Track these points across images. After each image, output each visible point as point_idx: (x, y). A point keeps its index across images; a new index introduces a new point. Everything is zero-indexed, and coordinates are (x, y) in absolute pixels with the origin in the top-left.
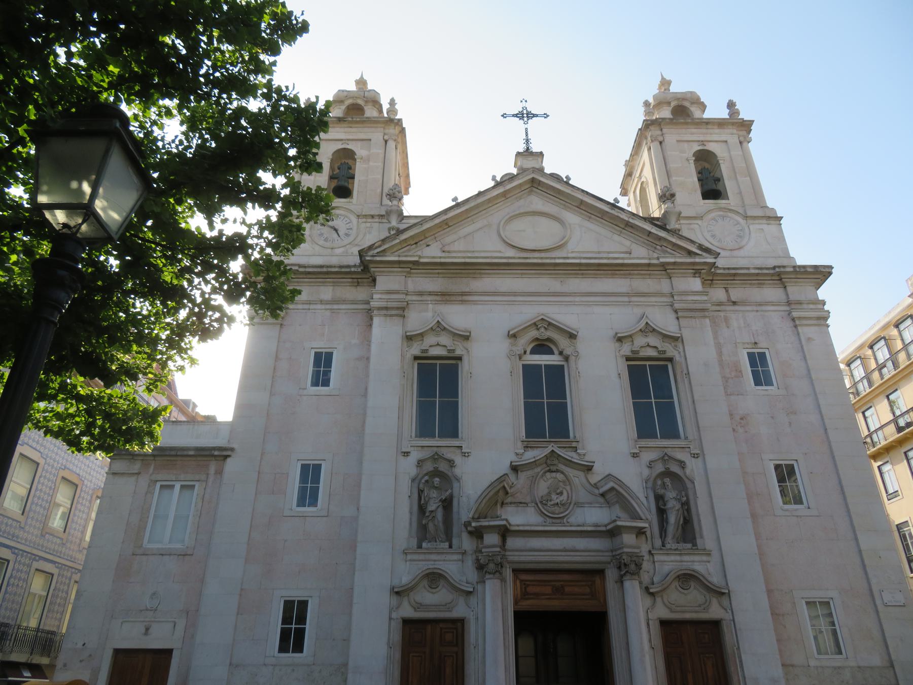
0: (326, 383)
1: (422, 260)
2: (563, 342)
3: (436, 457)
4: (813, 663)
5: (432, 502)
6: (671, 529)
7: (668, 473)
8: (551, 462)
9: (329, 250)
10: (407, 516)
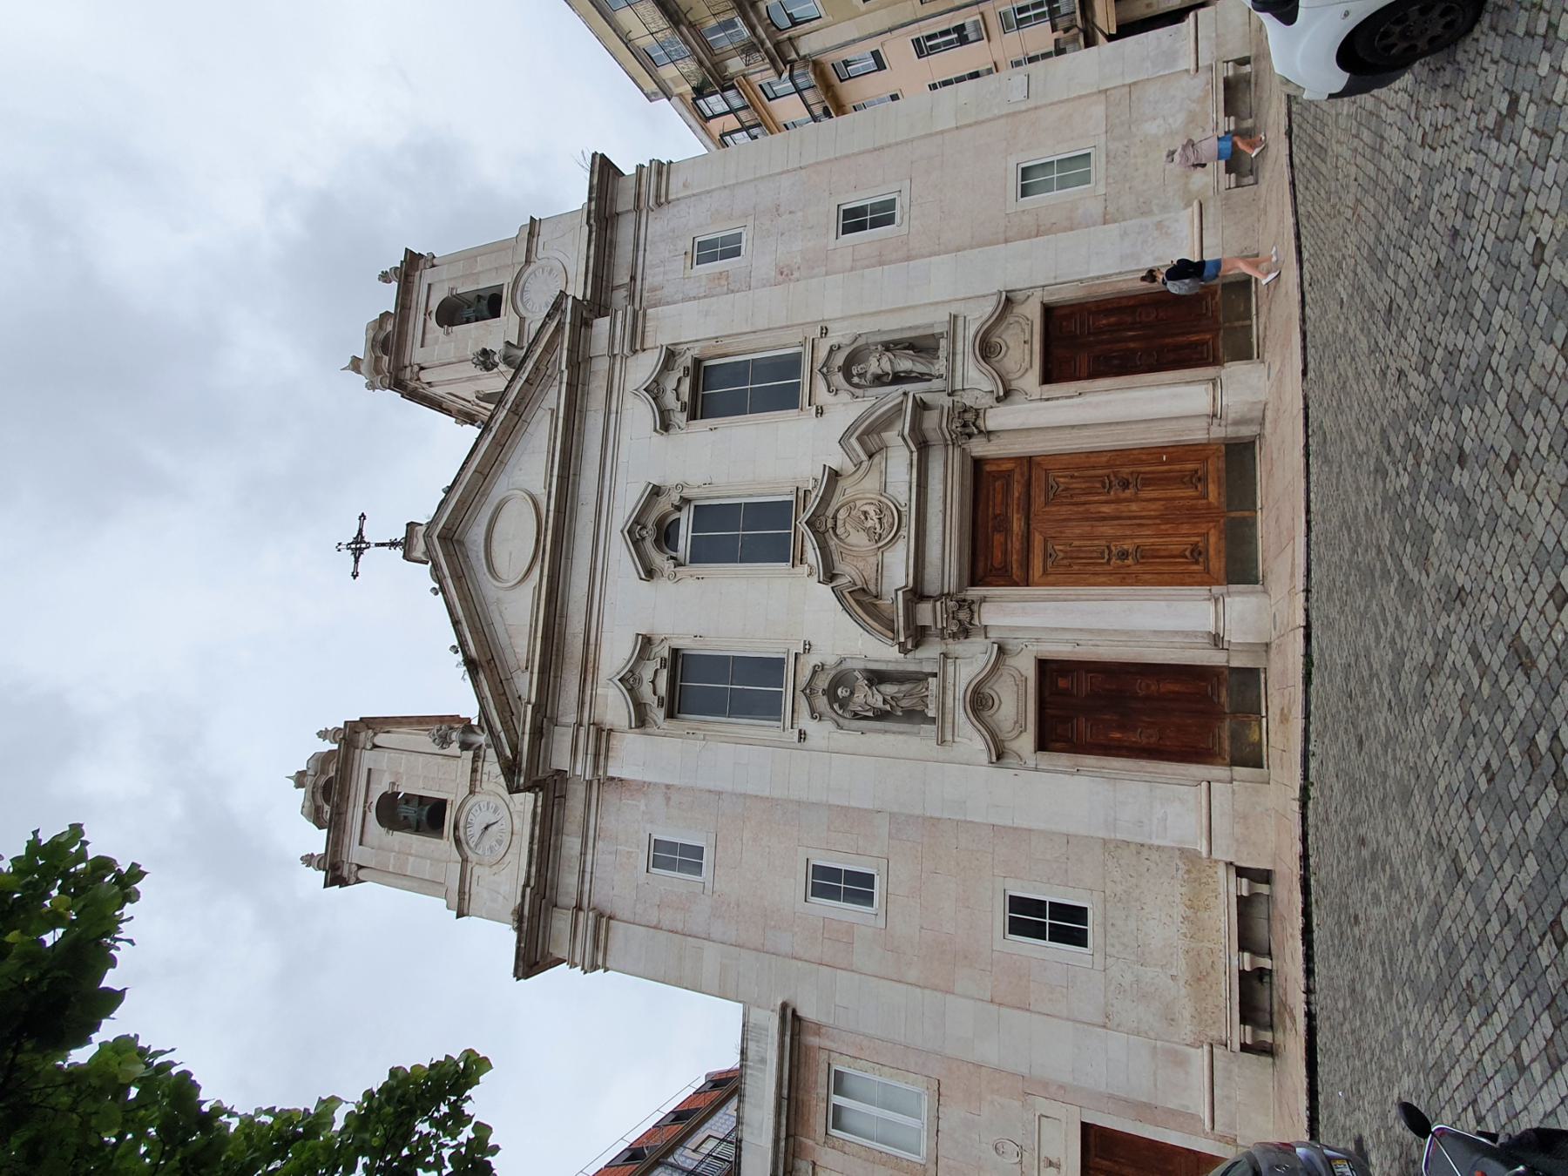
0: (698, 852)
2: (664, 505)
3: (809, 691)
4: (1102, 190)
6: (920, 368)
7: (846, 370)
10: (890, 737)
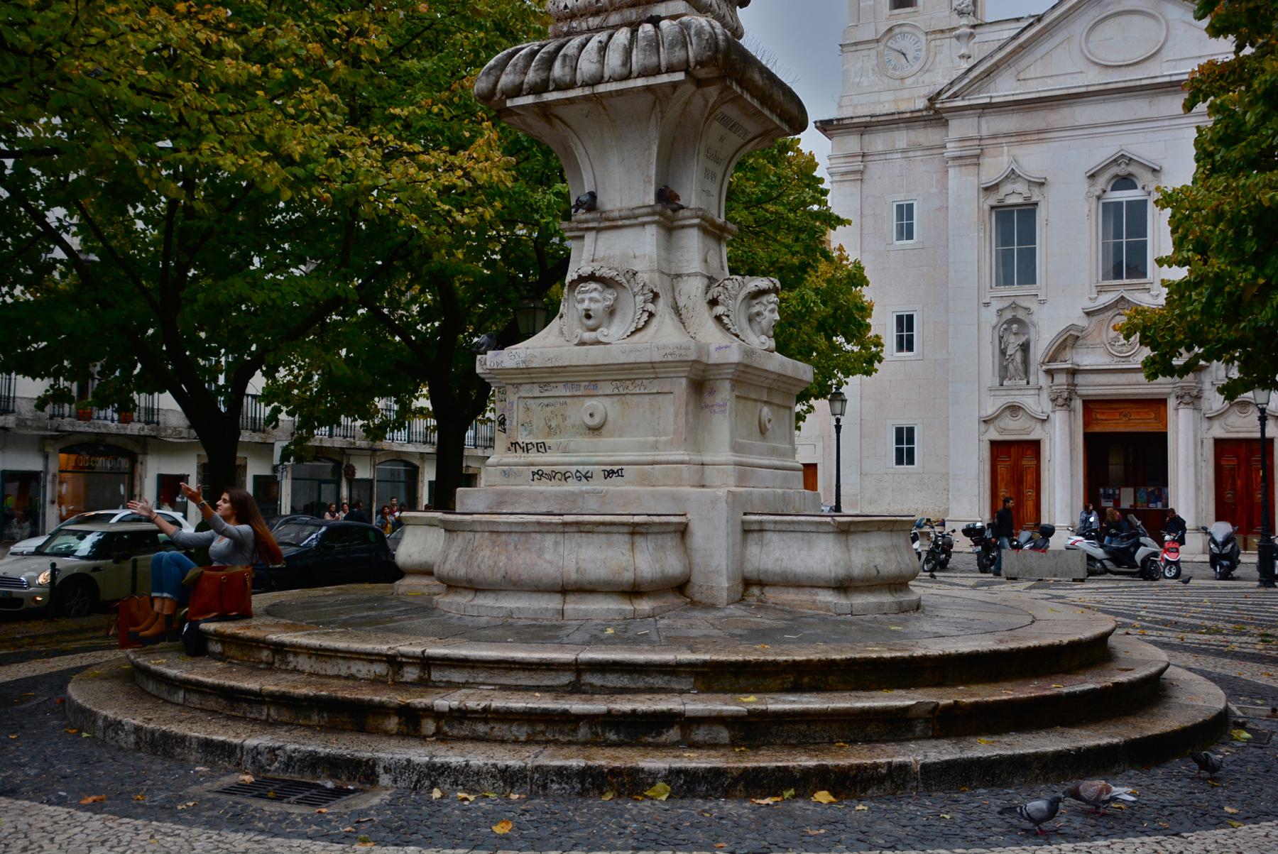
0: (910, 237)
1: (994, 100)
3: (1014, 306)
5: (1010, 347)
9: (898, 82)
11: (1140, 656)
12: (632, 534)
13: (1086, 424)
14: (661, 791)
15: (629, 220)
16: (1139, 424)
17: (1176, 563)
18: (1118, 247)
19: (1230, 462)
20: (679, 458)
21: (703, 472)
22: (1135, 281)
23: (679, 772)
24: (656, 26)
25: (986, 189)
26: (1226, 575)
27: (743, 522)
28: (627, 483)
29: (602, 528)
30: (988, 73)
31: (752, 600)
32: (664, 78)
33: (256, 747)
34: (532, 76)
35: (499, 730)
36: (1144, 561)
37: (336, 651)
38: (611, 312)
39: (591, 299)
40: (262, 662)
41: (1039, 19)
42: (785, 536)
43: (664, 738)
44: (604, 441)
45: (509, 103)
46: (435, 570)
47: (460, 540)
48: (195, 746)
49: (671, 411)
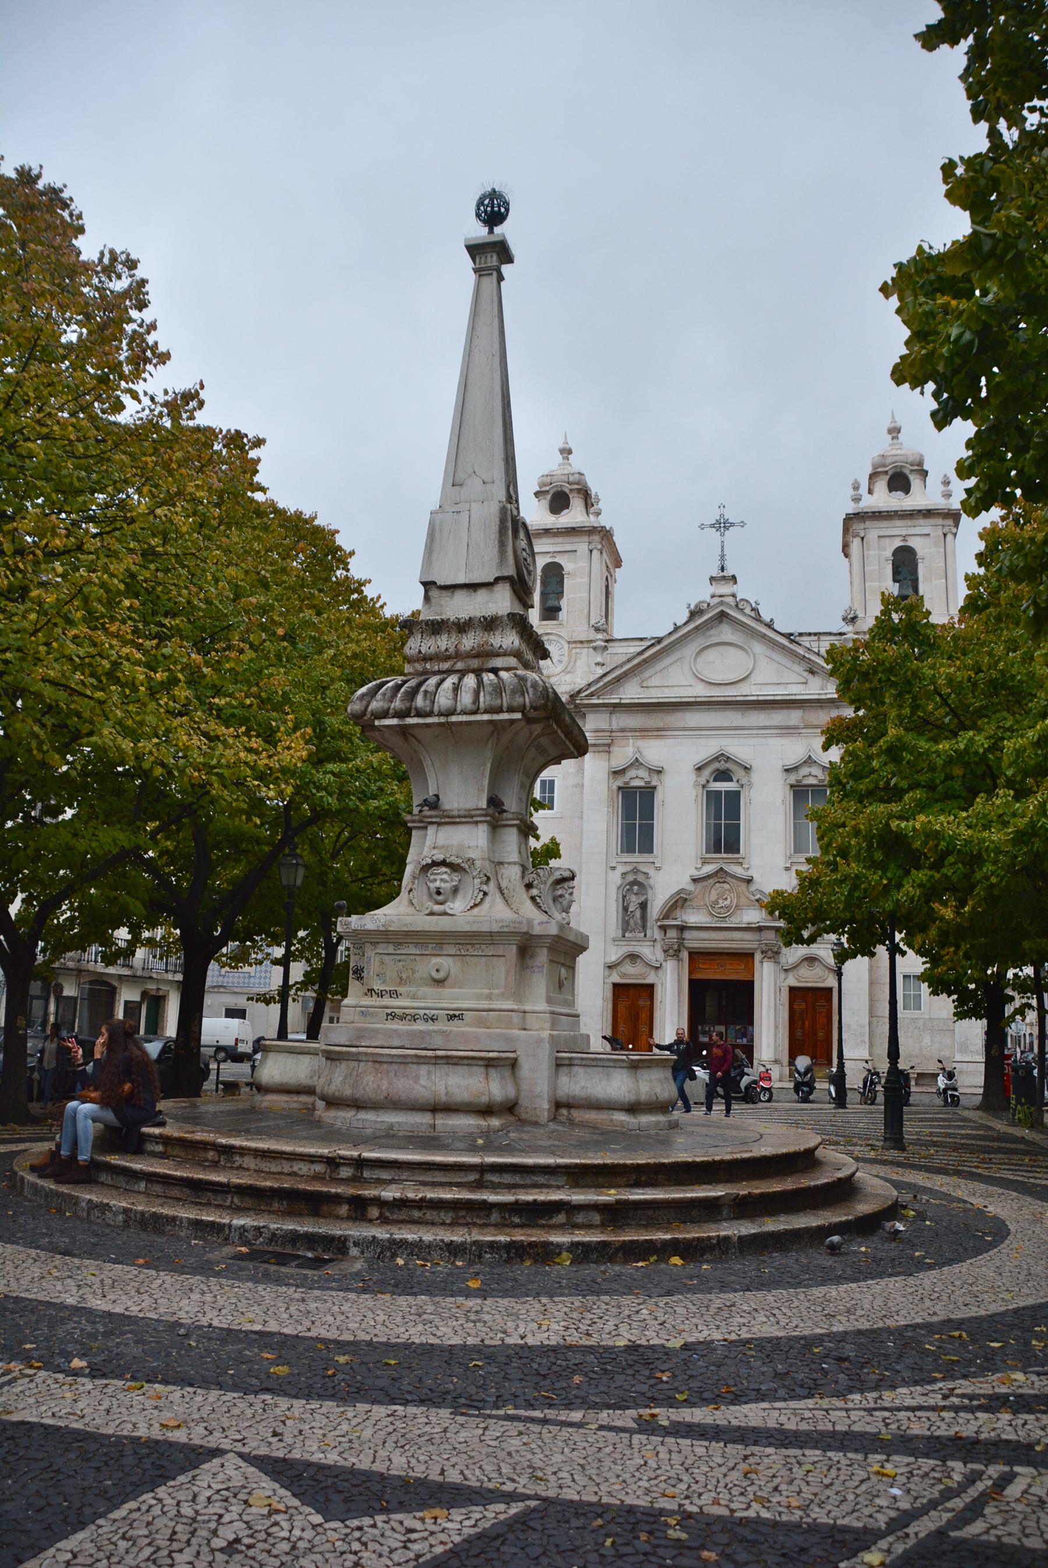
8: (720, 874)
11: (839, 1162)
12: (487, 1066)
13: (691, 972)
14: (566, 1259)
15: (467, 818)
16: (731, 973)
17: (769, 1089)
18: (718, 827)
19: (800, 1006)
20: (510, 1007)
21: (524, 1019)
22: (730, 856)
23: (578, 1244)
24: (496, 675)
25: (615, 773)
26: (805, 1100)
27: (557, 1058)
28: (466, 1025)
29: (465, 1062)
30: (618, 680)
31: (563, 1119)
32: (505, 716)
33: (243, 1226)
34: (397, 704)
35: (430, 1215)
36: (746, 1088)
37: (283, 1153)
38: (455, 890)
39: (442, 880)
40: (207, 1160)
41: (659, 640)
42: (589, 1070)
43: (554, 1221)
44: (447, 991)
45: (377, 723)
46: (318, 1090)
47: (343, 1068)
48: (185, 1224)
49: (503, 970)
